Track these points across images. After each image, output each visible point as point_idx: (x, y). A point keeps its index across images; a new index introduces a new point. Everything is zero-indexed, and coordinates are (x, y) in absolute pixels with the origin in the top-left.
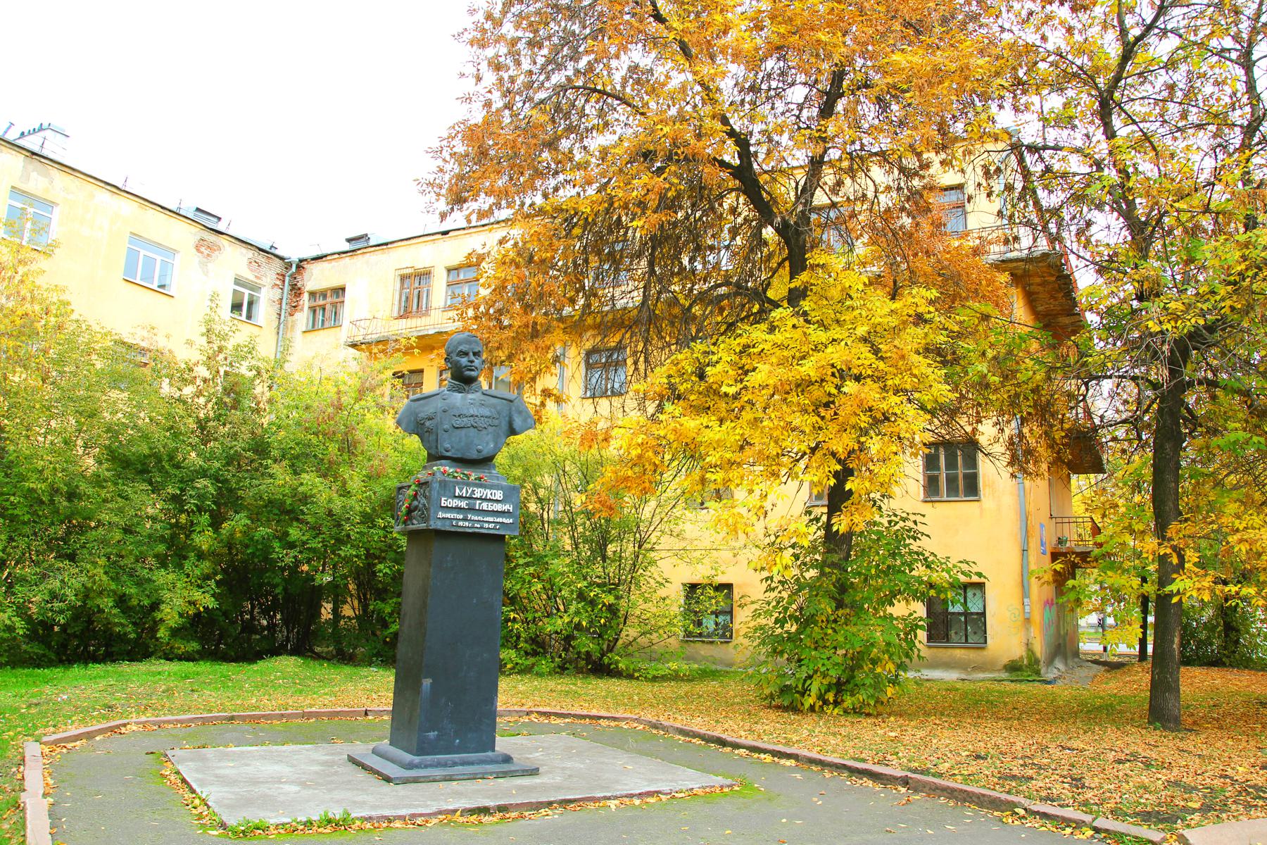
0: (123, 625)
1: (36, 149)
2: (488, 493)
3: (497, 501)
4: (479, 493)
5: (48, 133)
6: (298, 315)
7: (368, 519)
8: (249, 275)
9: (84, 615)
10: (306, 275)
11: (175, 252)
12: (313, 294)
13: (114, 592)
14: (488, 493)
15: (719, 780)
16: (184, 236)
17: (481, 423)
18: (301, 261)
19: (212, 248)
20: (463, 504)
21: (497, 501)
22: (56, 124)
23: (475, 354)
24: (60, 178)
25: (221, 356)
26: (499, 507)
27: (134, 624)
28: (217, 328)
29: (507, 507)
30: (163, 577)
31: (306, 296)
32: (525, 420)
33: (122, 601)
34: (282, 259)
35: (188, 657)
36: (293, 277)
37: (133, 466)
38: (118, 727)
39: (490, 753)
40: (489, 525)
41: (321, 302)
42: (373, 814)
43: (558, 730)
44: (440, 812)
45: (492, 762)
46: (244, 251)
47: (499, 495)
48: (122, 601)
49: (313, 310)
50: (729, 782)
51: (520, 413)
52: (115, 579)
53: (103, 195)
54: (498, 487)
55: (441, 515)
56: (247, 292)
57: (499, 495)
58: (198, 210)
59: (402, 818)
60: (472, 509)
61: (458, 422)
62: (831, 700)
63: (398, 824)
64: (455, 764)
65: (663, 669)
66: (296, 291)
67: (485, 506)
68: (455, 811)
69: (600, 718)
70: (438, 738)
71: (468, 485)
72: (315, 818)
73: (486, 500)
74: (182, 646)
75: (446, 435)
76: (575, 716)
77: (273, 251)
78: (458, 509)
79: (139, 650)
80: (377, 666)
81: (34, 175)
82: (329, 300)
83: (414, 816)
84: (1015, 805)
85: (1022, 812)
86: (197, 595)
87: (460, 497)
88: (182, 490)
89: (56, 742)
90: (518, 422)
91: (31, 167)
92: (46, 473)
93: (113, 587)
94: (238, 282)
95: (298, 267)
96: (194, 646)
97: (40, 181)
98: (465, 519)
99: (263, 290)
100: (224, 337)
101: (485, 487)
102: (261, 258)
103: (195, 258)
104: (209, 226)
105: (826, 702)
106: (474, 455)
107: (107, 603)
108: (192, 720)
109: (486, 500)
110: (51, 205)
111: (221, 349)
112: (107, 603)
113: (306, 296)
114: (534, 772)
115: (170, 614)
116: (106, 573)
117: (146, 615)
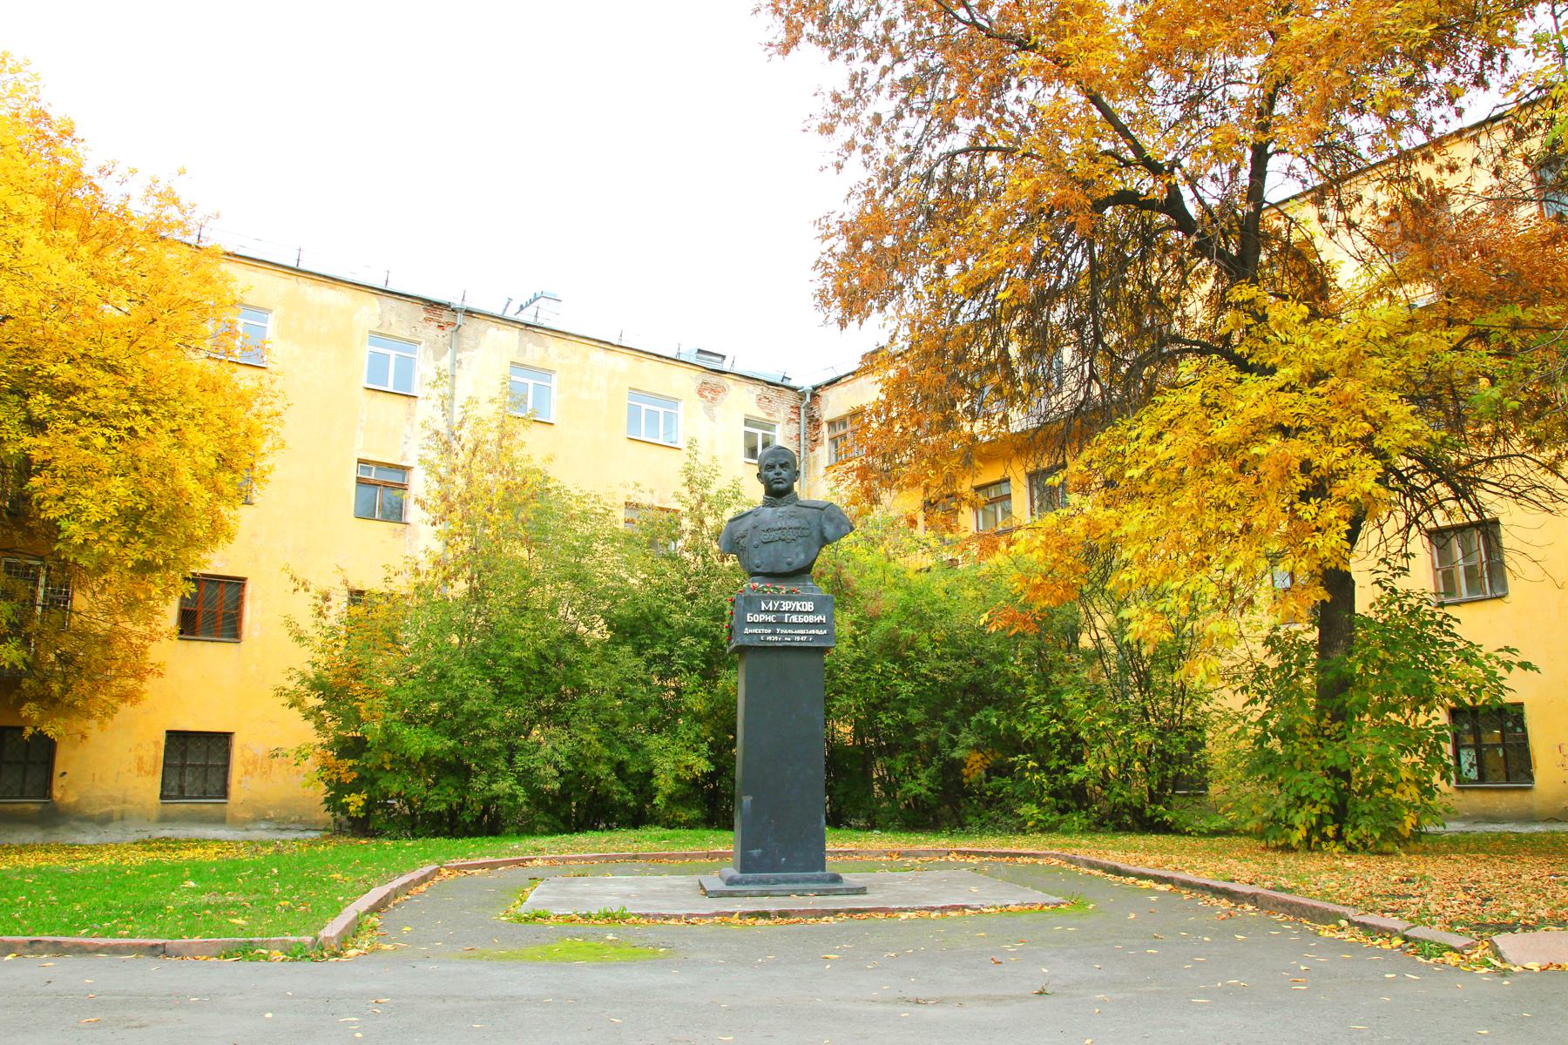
0: (619, 792)
1: (531, 321)
2: (797, 605)
3: (808, 613)
4: (786, 606)
5: (541, 302)
6: (819, 450)
7: (862, 664)
8: (761, 414)
9: (575, 778)
10: (822, 403)
11: (676, 401)
12: (831, 424)
13: (610, 759)
14: (797, 605)
15: (1038, 897)
16: (684, 382)
17: (790, 535)
18: (815, 388)
19: (717, 390)
20: (771, 618)
21: (808, 613)
22: (549, 291)
23: (782, 466)
24: (555, 345)
25: (705, 505)
26: (810, 619)
27: (634, 792)
28: (698, 475)
29: (819, 618)
30: (654, 742)
31: (825, 427)
32: (838, 528)
33: (620, 768)
34: (794, 389)
35: (690, 825)
36: (809, 408)
37: (636, 629)
38: (524, 861)
39: (819, 873)
40: (801, 637)
41: (842, 431)
42: (651, 912)
43: (958, 866)
44: (717, 914)
45: (818, 880)
46: (751, 387)
47: (809, 606)
48: (620, 768)
49: (833, 440)
50: (1055, 899)
51: (831, 520)
52: (609, 746)
53: (597, 355)
54: (807, 599)
55: (747, 631)
56: (760, 432)
57: (809, 606)
58: (700, 351)
59: (678, 917)
60: (780, 623)
61: (767, 537)
62: (1330, 834)
63: (672, 922)
64: (778, 882)
65: (1219, 823)
66: (814, 422)
67: (794, 618)
68: (733, 914)
69: (1019, 855)
70: (763, 855)
71: (775, 598)
72: (594, 912)
73: (795, 612)
74: (685, 815)
75: (756, 552)
76: (995, 854)
77: (786, 383)
78: (765, 624)
79: (637, 819)
80: (894, 830)
81: (530, 346)
82: (849, 428)
83: (690, 916)
84: (1339, 916)
85: (1343, 923)
86: (691, 759)
87: (767, 612)
88: (671, 651)
89: (458, 868)
90: (829, 530)
91: (526, 339)
92: (528, 641)
93: (607, 753)
94: (747, 422)
95: (813, 396)
96: (695, 813)
97: (536, 352)
98: (774, 633)
99: (778, 428)
100: (706, 485)
101: (794, 599)
102: (771, 393)
103: (699, 403)
104: (712, 370)
105: (1324, 837)
106: (784, 568)
107: (603, 770)
108: (596, 858)
109: (795, 612)
110: (548, 372)
111: (703, 500)
112: (603, 770)
113: (825, 427)
114: (861, 891)
115: (665, 783)
116: (600, 741)
117: (643, 783)
